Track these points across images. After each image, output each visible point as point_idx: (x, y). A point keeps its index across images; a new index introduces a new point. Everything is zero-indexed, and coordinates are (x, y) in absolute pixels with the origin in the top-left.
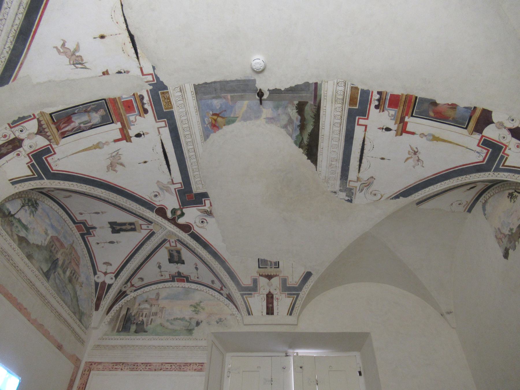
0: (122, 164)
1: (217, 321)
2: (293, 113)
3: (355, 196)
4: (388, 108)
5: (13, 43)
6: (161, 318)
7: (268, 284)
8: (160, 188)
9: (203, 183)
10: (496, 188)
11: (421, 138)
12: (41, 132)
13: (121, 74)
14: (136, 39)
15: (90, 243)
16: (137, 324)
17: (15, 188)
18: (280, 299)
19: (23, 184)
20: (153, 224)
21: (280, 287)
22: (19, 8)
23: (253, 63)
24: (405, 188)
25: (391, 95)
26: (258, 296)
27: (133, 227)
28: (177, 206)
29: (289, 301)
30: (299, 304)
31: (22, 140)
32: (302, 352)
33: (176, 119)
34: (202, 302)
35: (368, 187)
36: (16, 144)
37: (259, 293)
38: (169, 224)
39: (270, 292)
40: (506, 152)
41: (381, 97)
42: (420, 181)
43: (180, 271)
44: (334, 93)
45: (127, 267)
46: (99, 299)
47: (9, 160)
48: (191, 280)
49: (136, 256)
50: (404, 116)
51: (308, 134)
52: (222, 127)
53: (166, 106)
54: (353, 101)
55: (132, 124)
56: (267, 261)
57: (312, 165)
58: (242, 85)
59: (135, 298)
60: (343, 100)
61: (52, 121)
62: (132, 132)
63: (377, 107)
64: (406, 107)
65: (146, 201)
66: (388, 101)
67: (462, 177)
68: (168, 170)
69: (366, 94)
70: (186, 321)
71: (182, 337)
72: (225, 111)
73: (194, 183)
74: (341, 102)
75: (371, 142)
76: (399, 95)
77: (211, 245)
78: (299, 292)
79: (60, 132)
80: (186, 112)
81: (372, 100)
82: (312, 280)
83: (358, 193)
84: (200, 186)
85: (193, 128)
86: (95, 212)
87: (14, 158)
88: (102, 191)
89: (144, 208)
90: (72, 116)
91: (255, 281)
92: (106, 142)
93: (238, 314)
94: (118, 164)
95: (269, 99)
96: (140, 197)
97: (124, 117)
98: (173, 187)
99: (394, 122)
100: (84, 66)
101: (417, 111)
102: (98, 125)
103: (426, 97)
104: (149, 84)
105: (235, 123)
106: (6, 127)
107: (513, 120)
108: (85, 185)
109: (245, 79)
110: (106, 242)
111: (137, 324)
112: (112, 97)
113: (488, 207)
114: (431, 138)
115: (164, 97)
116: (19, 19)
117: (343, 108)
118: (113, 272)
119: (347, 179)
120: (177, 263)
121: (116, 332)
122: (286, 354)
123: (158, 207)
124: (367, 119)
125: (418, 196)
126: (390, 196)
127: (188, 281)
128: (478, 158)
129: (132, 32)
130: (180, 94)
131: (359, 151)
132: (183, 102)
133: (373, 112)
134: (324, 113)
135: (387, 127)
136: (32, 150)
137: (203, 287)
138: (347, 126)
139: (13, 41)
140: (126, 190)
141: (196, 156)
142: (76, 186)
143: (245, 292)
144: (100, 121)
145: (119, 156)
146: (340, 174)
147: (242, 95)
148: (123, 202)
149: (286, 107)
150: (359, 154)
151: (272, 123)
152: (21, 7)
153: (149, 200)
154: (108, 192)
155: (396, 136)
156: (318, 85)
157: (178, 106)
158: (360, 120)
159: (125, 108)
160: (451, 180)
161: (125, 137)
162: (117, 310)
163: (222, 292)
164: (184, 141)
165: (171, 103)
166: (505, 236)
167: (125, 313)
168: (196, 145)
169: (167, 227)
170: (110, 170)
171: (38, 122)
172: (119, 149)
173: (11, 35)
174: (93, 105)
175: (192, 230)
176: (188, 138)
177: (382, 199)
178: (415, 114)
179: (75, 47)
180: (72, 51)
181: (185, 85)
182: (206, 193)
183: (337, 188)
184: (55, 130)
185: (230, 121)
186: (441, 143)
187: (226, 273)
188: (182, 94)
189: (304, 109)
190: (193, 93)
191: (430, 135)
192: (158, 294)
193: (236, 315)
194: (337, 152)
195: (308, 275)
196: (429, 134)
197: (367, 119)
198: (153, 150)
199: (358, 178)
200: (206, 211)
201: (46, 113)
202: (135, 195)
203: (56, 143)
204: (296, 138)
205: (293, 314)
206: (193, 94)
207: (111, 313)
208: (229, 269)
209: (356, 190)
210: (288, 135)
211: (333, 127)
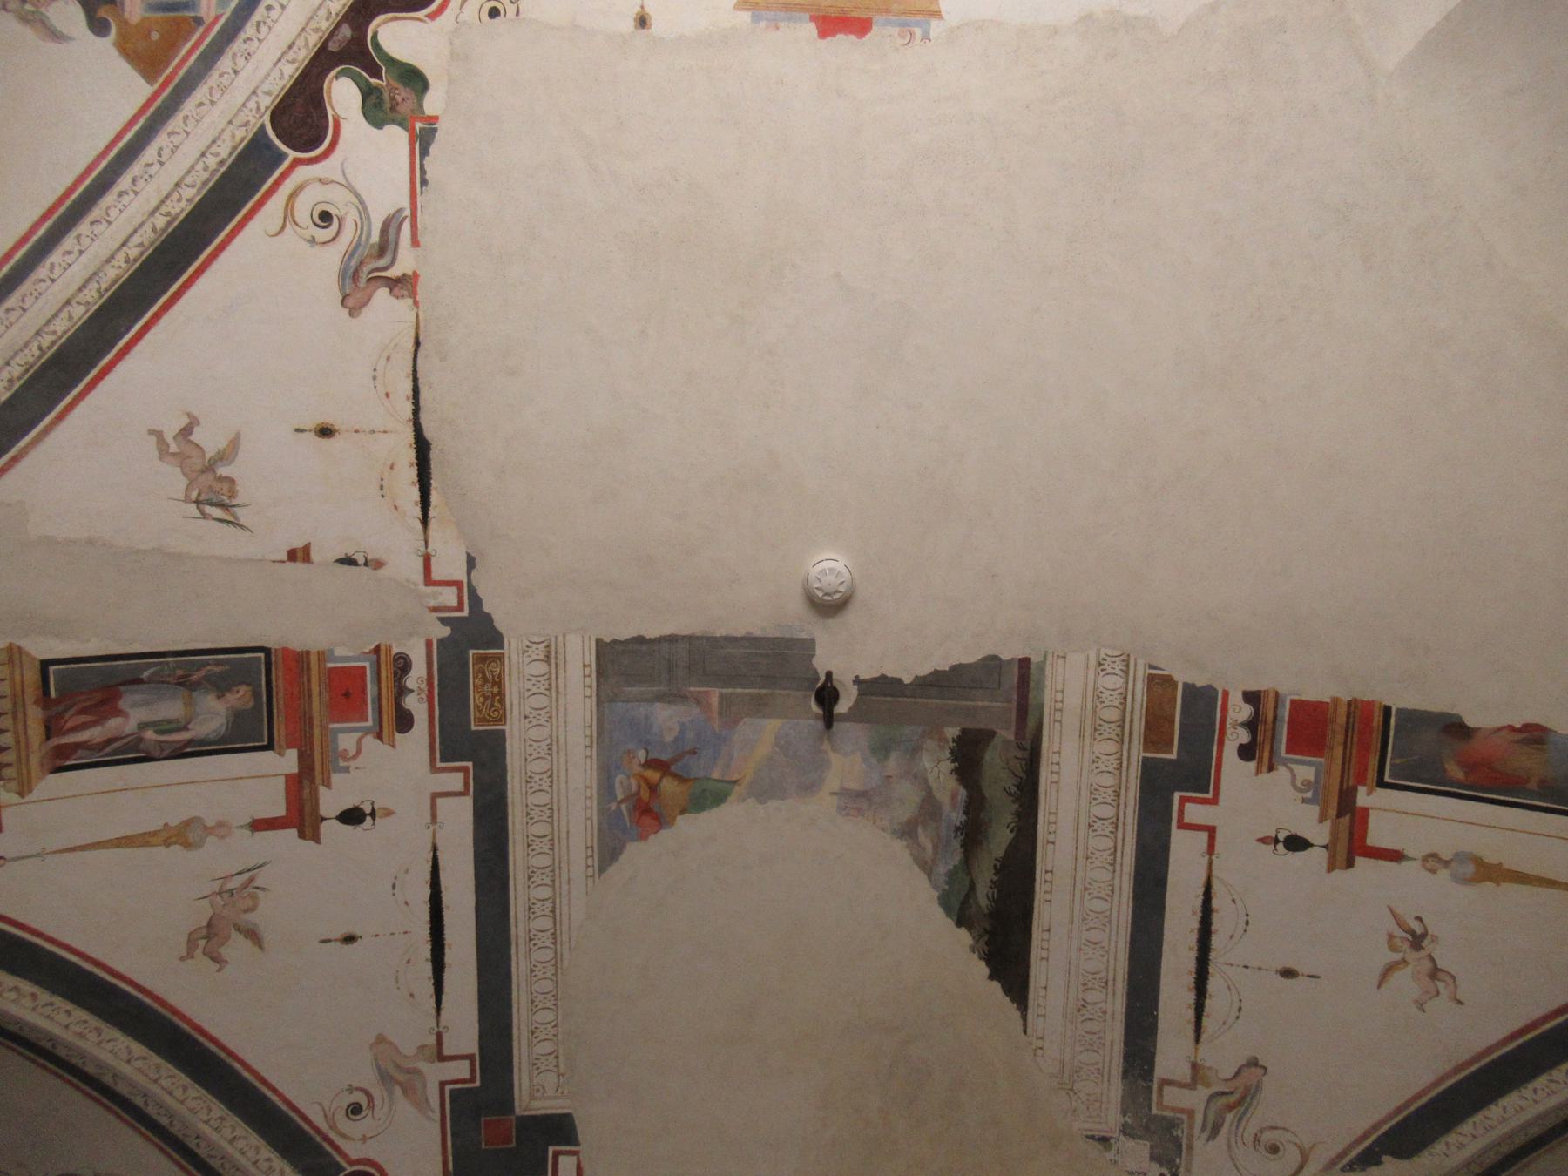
0: (253, 935)
2: (942, 776)
5: (17, 385)
9: (562, 1070)
11: (1428, 874)
13: (354, 568)
14: (434, 455)
22: (84, 286)
23: (814, 572)
24: (1399, 1110)
25: (1293, 702)
33: (509, 768)
35: (1242, 1109)
41: (1257, 713)
44: (1090, 699)
50: (1351, 783)
51: (995, 866)
52: (674, 819)
53: (480, 711)
54: (1156, 729)
55: (342, 763)
60: (1122, 727)
62: (331, 801)
63: (1246, 752)
65: (303, 1131)
66: (1285, 726)
68: (431, 990)
69: (1202, 701)
72: (694, 752)
73: (525, 1066)
74: (1113, 736)
76: (1322, 703)
79: (55, 741)
80: (551, 744)
81: (1228, 726)
83: (1199, 1144)
84: (550, 1080)
85: (564, 813)
88: (130, 1052)
90: (122, 688)
92: (220, 824)
94: (238, 930)
95: (856, 714)
96: (284, 1107)
97: (317, 731)
98: (435, 1073)
100: (234, 515)
101: (1398, 761)
102: (211, 744)
108: (70, 1006)
109: (778, 635)
112: (296, 645)
114: (1470, 869)
115: (484, 674)
116: (70, 318)
117: (1120, 759)
119: (1148, 1073)
123: (349, 1169)
124: (1214, 801)
125: (1461, 1146)
129: (429, 434)
130: (542, 668)
131: (1193, 938)
133: (1234, 772)
134: (1055, 777)
135: (1293, 832)
139: (19, 378)
140: (237, 1066)
142: (27, 1002)
144: (222, 733)
145: (254, 897)
146: (1119, 1048)
148: (206, 1122)
149: (915, 751)
150: (1194, 954)
152: (94, 286)
153: (323, 1126)
156: (1033, 667)
157: (526, 717)
158: (1189, 806)
159: (331, 698)
165: (502, 701)
168: (565, 887)
170: (199, 951)
173: (20, 359)
174: (218, 663)
178: (1390, 777)
179: (222, 444)
180: (208, 456)
181: (567, 637)
183: (1112, 1119)
184: (35, 731)
185: (706, 798)
188: (550, 672)
190: (587, 671)
191: (1461, 857)
194: (1105, 944)
196: (1457, 854)
197: (1214, 801)
198: (394, 887)
199: (1195, 1067)
201: (28, 655)
203: (21, 784)
204: (947, 883)
206: (590, 676)
209: (1191, 1127)
210: (916, 869)
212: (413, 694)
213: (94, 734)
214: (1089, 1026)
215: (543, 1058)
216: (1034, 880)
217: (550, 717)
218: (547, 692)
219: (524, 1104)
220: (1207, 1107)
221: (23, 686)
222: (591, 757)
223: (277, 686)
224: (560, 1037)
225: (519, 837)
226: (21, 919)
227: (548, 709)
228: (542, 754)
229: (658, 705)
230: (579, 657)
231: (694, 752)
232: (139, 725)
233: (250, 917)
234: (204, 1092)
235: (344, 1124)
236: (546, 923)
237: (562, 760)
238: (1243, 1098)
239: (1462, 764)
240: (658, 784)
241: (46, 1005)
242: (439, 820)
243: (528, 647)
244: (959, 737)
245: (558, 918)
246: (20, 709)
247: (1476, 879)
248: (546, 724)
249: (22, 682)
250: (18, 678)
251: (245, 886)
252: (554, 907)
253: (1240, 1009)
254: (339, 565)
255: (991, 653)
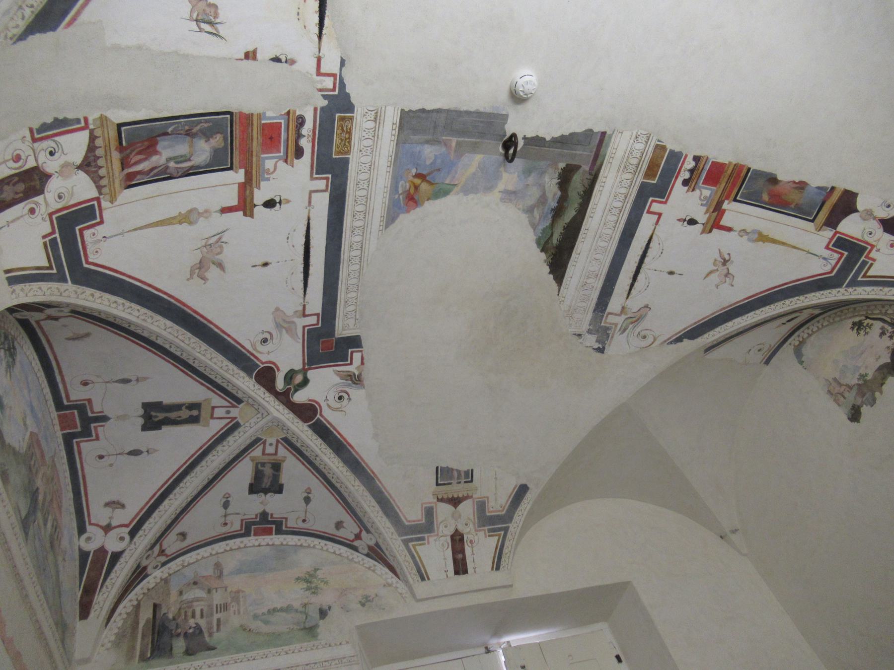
0: (220, 266)
1: (360, 602)
3: (611, 342)
4: (703, 186)
6: (239, 613)
7: (453, 516)
8: (276, 323)
9: (357, 317)
10: (824, 318)
12: (89, 165)
15: (81, 458)
16: (186, 635)
17: (12, 292)
18: (476, 540)
19: (27, 286)
20: (241, 406)
21: (474, 519)
23: (521, 82)
26: (435, 540)
27: (195, 413)
28: (298, 366)
29: (493, 542)
30: (510, 547)
31: (49, 176)
32: (516, 639)
33: (349, 178)
34: (318, 569)
35: (636, 323)
36: (33, 184)
37: (438, 535)
38: (277, 403)
39: (457, 530)
40: (871, 255)
41: (696, 166)
42: (721, 310)
43: (268, 510)
45: (161, 508)
46: (89, 592)
47: (13, 221)
48: (286, 527)
49: (185, 481)
53: (338, 148)
54: (651, 170)
55: (266, 176)
56: (452, 469)
57: (554, 285)
58: (482, 122)
59: (166, 581)
61: (117, 143)
62: (260, 196)
63: (686, 183)
64: (730, 185)
67: (791, 299)
69: (676, 157)
70: (297, 611)
71: (298, 646)
75: (661, 244)
77: (350, 445)
78: (507, 525)
80: (371, 165)
81: (682, 170)
82: (529, 499)
83: (616, 336)
84: (351, 322)
86: (122, 377)
87: (22, 216)
89: (235, 368)
90: (158, 139)
91: (429, 513)
92: (206, 211)
93: (397, 582)
94: (214, 263)
97: (254, 159)
98: (301, 322)
99: (704, 209)
100: (216, 29)
101: (745, 191)
103: (761, 169)
104: (322, 95)
105: (448, 196)
106: (25, 137)
107: (889, 206)
108: (139, 307)
110: (121, 454)
111: (186, 635)
112: (246, 111)
113: (807, 351)
114: (756, 236)
117: (632, 182)
118: (127, 522)
119: (604, 311)
120: (266, 491)
121: (139, 663)
122: (486, 648)
123: (262, 366)
126: (668, 339)
127: (279, 531)
128: (823, 268)
130: (371, 125)
132: (372, 144)
133: (678, 190)
136: (60, 206)
137: (312, 539)
138: (629, 215)
140: (212, 326)
141: (361, 258)
142: (121, 307)
143: (411, 537)
144: (208, 161)
145: (221, 247)
147: (476, 143)
148: (199, 353)
149: (543, 173)
151: (510, 200)
153: (250, 349)
154: (177, 327)
155: (702, 233)
156: (606, 136)
157: (361, 151)
159: (263, 140)
160: (772, 306)
161: (245, 206)
162: (128, 614)
163: (356, 543)
164: (349, 225)
165: (350, 142)
166: (850, 388)
167: (151, 616)
169: (272, 410)
171: (90, 138)
172: (225, 229)
174: (206, 121)
175: (318, 416)
176: (358, 218)
177: (653, 345)
181: (387, 108)
182: (359, 336)
183: (585, 326)
184: (117, 165)
185: (441, 193)
186: (770, 247)
187: (374, 503)
188: (375, 127)
189: (571, 178)
191: (754, 231)
192: (218, 566)
193: (394, 585)
195: (522, 490)
196: (753, 230)
198: (288, 238)
199: (623, 308)
200: (350, 376)
201: (111, 121)
202: (226, 337)
204: (541, 233)
205: (501, 567)
206: (395, 130)
207: (115, 621)
208: (381, 492)
211: (607, 216)
212: (304, 138)
213: (144, 166)
214: (586, 292)
215: (350, 313)
216: (579, 232)
217: (372, 151)
218: (373, 138)
219: (339, 332)
220: (623, 322)
221: (109, 140)
222: (389, 172)
223: (236, 134)
224: (358, 303)
225: (349, 212)
226: (115, 268)
227: (372, 147)
228: (366, 171)
229: (426, 146)
230: (391, 117)
231: (439, 170)
232: (167, 159)
233: (219, 257)
234: (197, 339)
235: (260, 348)
236: (358, 253)
237: (375, 174)
238: (638, 319)
239: (769, 194)
240: (419, 186)
241: (129, 308)
242: (312, 204)
243: (366, 113)
244: (564, 168)
245: (363, 250)
246: (109, 154)
247: (757, 240)
248: (370, 154)
249: (109, 137)
250: (106, 136)
251: (217, 242)
252: (362, 245)
253: (648, 286)
254: (272, 62)
255: (590, 128)
